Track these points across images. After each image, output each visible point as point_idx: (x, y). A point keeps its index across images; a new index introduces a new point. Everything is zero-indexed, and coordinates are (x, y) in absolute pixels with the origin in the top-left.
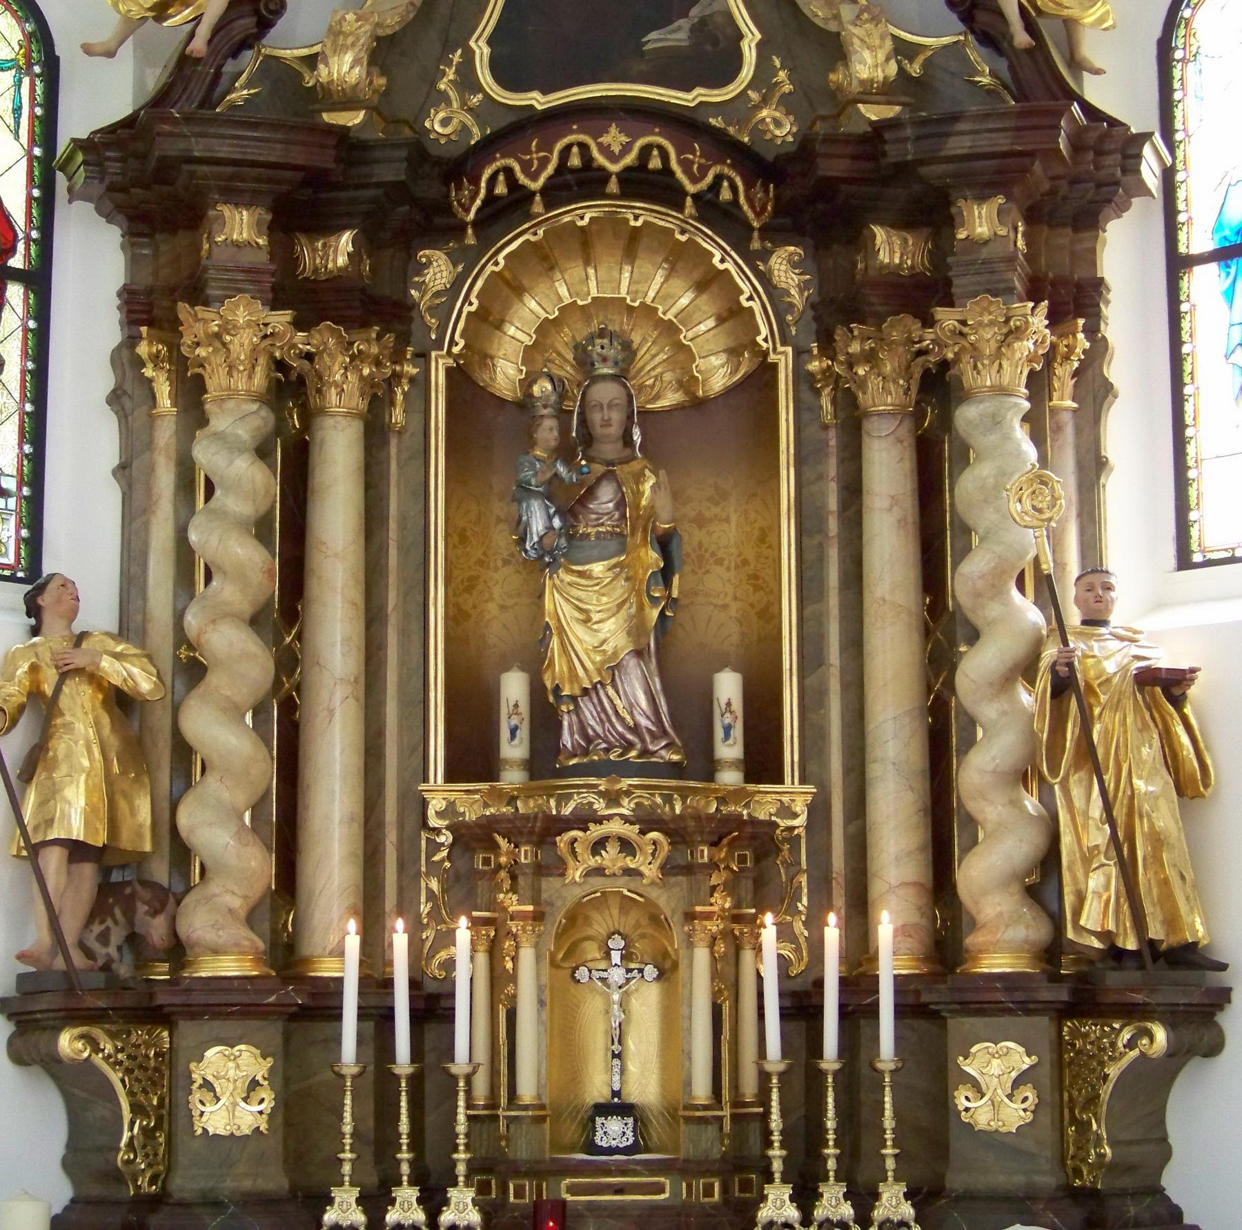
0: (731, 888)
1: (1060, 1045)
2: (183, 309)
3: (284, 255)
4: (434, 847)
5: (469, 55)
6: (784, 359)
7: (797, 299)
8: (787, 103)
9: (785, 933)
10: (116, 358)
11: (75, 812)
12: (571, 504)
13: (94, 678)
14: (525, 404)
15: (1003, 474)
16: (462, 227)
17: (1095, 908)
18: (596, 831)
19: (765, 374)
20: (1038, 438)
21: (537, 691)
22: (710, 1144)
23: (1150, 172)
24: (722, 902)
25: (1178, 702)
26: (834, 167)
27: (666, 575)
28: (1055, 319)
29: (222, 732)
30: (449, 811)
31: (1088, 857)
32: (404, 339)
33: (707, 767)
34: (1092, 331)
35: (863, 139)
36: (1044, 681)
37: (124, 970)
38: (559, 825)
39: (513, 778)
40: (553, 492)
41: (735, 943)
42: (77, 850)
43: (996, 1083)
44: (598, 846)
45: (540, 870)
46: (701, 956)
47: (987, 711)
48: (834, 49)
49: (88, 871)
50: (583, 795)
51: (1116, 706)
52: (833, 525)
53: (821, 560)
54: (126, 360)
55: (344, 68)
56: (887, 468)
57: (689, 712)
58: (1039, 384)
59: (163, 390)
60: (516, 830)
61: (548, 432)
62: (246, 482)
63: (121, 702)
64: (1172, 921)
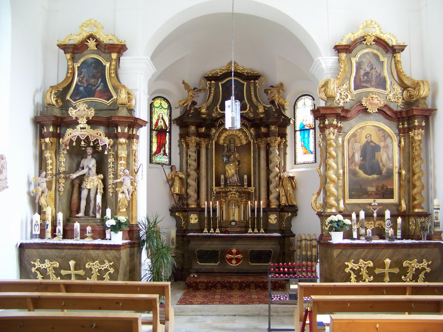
0: (245, 198)
1: (280, 215)
2: (187, 137)
3: (197, 131)
4: (214, 194)
5: (217, 107)
6: (252, 141)
7: (253, 134)
8: (252, 113)
9: (251, 203)
10: (179, 141)
11: (177, 190)
12: (229, 157)
13: (178, 176)
14: (223, 146)
15: (275, 155)
16: (216, 127)
17: (283, 201)
18: (231, 193)
19: (250, 142)
20: (279, 151)
21: (225, 177)
22: (243, 225)
23: (292, 122)
24: (245, 200)
25: (293, 180)
26: (257, 122)
27: (239, 165)
28: (281, 138)
29: (192, 182)
30: (215, 190)
31: (283, 196)
32: (210, 139)
33: (243, 185)
34: (285, 139)
35: (260, 119)
36: (278, 178)
37: (182, 206)
38: (227, 192)
39: (222, 186)
40: (226, 156)
41: (246, 204)
42: (177, 194)
43: (273, 219)
44: (232, 194)
45: (226, 196)
46: (242, 206)
47: (273, 180)
48: (257, 108)
49: (178, 196)
50: (230, 188)
51: (286, 180)
52: (257, 159)
53: (256, 163)
54: (180, 141)
55: (203, 111)
56: (263, 154)
57: (241, 179)
58: (279, 145)
59: (184, 145)
60: (223, 192)
61: (226, 149)
62: (194, 155)
63: (181, 179)
64: (292, 202)
